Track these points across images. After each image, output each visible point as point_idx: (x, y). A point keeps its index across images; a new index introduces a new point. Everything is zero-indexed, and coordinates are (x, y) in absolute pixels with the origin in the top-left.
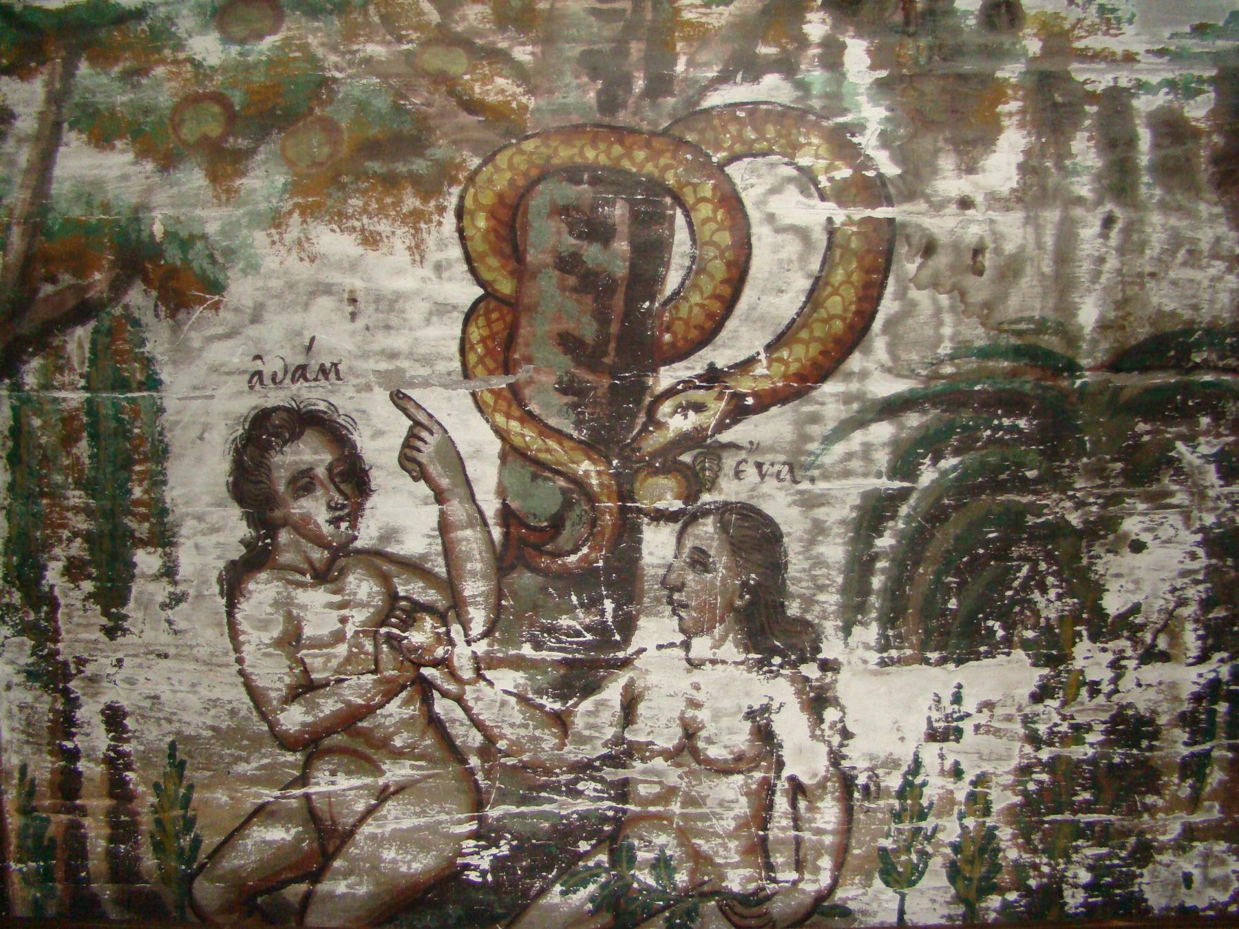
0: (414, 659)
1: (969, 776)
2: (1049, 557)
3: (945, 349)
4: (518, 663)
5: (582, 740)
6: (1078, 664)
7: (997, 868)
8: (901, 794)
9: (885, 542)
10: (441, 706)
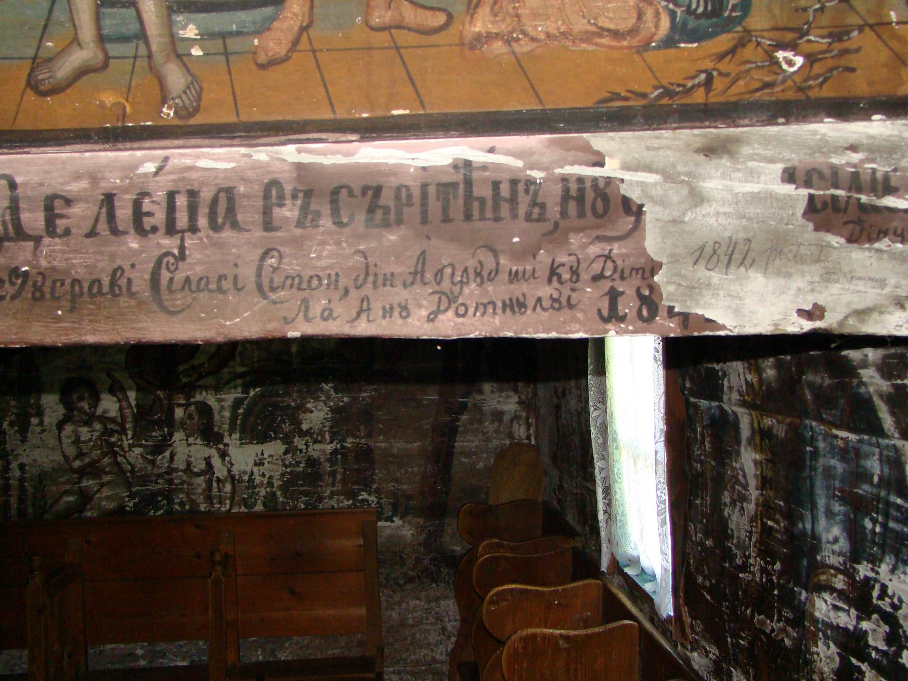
0: (112, 445)
1: (267, 476)
2: (286, 415)
3: (256, 359)
4: (141, 446)
5: (159, 467)
6: (296, 444)
7: (277, 503)
8: (248, 481)
9: (241, 411)
10: (119, 459)
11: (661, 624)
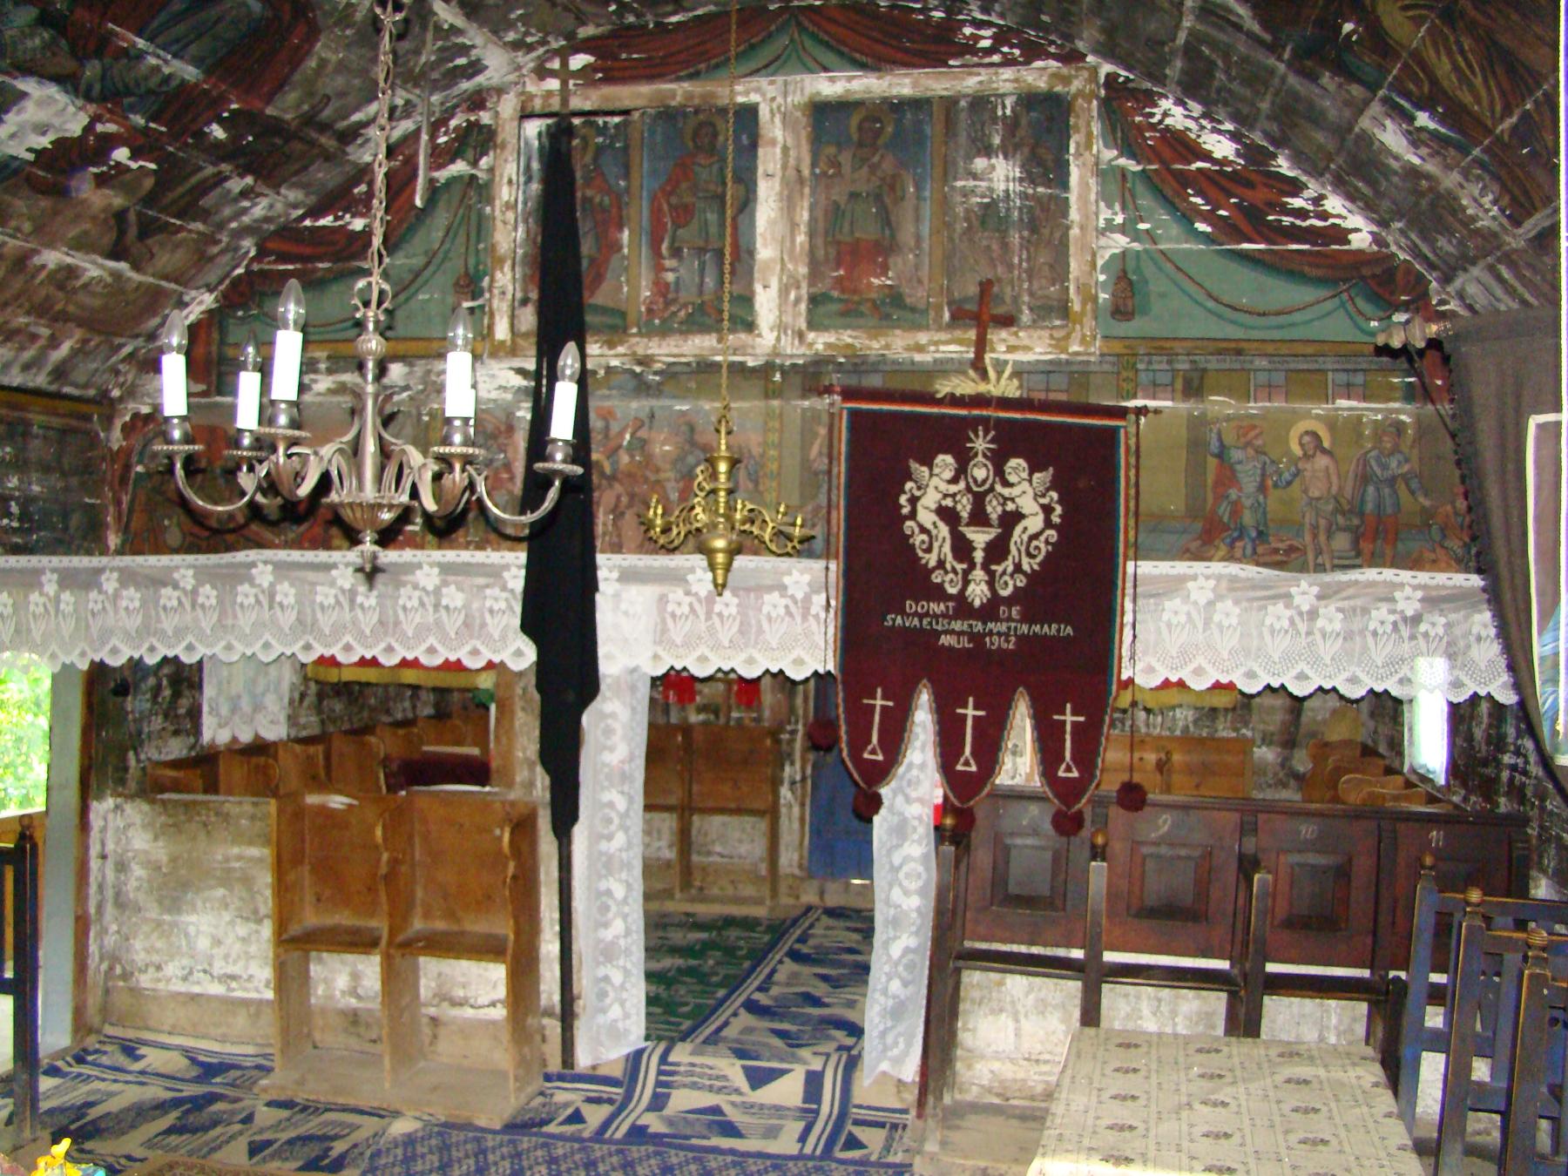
11: (1439, 789)
